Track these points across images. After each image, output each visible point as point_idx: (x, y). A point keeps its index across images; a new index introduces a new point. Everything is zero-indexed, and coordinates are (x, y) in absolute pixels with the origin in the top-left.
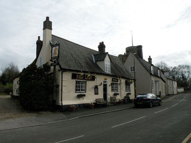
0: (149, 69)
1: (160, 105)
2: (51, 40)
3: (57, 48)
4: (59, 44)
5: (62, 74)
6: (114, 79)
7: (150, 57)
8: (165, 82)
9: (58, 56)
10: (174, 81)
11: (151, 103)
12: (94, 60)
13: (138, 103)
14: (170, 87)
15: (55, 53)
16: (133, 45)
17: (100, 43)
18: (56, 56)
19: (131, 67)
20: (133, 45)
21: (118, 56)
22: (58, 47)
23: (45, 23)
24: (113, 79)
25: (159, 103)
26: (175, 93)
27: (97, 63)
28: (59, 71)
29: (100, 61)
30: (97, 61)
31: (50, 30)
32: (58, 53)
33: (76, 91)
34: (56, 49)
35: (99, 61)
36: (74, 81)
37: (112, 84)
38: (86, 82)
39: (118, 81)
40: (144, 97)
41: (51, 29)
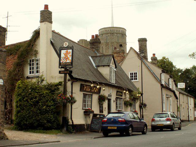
0: (159, 77)
1: (145, 134)
2: (51, 37)
3: (70, 52)
4: (73, 47)
5: (72, 84)
6: (119, 92)
7: (46, 7)
8: (177, 98)
9: (72, 63)
10: (189, 98)
11: (131, 129)
12: (94, 65)
13: (109, 128)
14: (183, 108)
15: (67, 59)
16: (113, 23)
17: (93, 36)
18: (68, 61)
19: (131, 74)
20: (113, 23)
21: (77, 42)
22: (71, 51)
23: (42, 13)
24: (117, 92)
25: (144, 130)
26: (192, 118)
27: (98, 70)
28: (69, 80)
29: (104, 66)
30: (99, 66)
31: (50, 24)
32: (71, 59)
33: (116, 109)
34: (67, 53)
35: (101, 66)
36: (82, 93)
37: (117, 98)
38: (92, 95)
39: (122, 96)
40: (120, 117)
41: (51, 22)
